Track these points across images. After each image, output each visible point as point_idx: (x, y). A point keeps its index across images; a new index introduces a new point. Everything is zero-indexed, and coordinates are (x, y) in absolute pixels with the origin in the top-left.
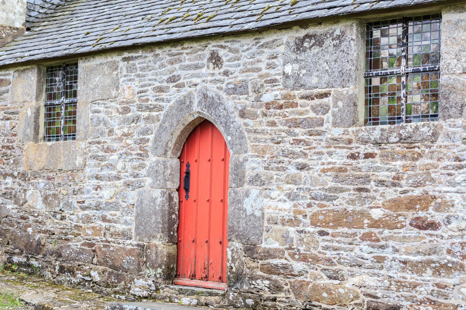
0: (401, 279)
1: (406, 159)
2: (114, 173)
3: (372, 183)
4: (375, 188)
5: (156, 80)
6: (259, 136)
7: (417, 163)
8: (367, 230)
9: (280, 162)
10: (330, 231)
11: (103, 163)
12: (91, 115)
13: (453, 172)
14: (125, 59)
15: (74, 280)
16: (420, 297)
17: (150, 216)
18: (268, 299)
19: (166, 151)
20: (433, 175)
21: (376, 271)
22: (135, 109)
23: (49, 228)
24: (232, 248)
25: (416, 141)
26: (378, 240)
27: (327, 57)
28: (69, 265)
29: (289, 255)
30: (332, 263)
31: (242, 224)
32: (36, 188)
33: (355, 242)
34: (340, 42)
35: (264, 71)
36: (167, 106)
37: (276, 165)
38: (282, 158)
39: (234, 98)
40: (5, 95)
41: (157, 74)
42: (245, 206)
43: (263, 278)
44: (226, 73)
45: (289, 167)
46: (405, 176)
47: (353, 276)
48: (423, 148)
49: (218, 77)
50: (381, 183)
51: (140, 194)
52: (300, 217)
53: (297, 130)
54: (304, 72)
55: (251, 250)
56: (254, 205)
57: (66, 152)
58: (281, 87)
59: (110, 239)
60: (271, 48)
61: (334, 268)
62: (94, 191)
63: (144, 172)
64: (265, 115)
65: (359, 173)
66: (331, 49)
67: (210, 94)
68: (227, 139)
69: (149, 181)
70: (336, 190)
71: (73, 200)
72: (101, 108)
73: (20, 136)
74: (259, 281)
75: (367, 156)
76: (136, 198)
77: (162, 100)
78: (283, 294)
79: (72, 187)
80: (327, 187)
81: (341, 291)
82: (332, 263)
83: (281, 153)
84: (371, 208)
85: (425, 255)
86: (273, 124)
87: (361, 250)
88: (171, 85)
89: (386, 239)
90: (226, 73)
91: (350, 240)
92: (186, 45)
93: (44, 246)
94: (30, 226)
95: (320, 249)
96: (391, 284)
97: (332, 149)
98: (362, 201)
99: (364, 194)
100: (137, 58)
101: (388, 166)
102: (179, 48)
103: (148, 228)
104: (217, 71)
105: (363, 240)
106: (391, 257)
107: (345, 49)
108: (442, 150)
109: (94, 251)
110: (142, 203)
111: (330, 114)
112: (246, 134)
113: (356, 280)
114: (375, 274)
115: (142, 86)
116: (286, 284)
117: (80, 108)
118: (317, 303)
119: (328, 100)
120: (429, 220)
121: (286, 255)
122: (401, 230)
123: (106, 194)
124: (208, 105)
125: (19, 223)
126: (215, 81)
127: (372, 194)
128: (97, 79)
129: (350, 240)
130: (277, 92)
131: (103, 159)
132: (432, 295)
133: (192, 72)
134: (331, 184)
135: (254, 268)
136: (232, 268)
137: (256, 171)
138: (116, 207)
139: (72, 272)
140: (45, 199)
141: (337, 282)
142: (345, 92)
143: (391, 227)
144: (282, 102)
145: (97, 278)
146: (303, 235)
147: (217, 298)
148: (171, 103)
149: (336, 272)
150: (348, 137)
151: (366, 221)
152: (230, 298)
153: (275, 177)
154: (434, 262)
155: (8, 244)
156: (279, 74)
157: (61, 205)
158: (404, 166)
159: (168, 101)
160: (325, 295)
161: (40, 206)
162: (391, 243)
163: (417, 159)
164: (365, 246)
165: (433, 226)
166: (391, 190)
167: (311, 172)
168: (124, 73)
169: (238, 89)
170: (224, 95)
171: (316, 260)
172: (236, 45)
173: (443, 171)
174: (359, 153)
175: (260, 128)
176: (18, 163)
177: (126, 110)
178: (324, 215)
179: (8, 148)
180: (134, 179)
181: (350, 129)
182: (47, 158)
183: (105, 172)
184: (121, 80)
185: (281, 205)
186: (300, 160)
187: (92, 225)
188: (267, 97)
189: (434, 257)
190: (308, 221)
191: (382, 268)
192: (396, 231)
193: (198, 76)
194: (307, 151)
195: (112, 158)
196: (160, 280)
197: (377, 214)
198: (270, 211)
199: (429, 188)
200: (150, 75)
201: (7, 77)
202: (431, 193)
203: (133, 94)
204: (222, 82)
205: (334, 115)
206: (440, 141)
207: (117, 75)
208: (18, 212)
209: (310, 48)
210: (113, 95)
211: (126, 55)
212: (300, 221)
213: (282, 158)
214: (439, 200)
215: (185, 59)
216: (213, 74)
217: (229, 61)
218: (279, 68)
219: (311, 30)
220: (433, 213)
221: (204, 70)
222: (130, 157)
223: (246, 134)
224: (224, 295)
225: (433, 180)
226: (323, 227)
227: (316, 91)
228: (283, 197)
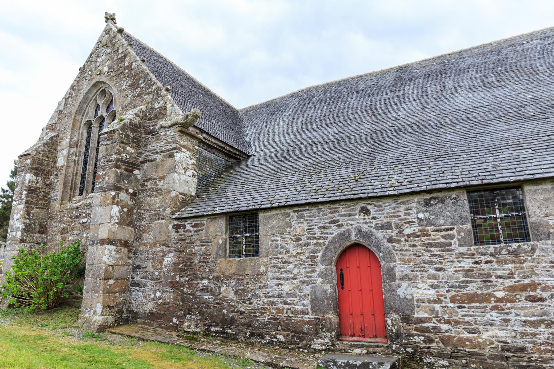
0: (524, 331)
1: (515, 263)
2: (292, 276)
3: (493, 277)
4: (496, 280)
5: (320, 222)
6: (404, 253)
7: (524, 265)
8: (494, 304)
9: (422, 267)
10: (466, 306)
11: (282, 270)
12: (270, 243)
13: (550, 269)
14: (295, 211)
15: (263, 341)
16: (539, 341)
17: (323, 301)
18: (424, 348)
19: (332, 262)
20: (537, 272)
21: (504, 327)
22: (305, 239)
23: (240, 309)
24: (391, 318)
25: (520, 253)
26: (503, 310)
27: (449, 209)
28: (259, 332)
29: (437, 320)
30: (470, 324)
31: (398, 303)
32: (229, 286)
33: (486, 311)
34: (457, 201)
35: (403, 217)
36: (330, 237)
37: (419, 269)
38: (423, 265)
39: (382, 232)
40: (201, 232)
41: (321, 219)
42: (398, 293)
43: (419, 335)
44: (374, 218)
45: (430, 270)
46: (517, 273)
47: (487, 331)
48: (526, 257)
49: (368, 220)
50: (500, 277)
51: (312, 288)
52: (442, 298)
53: (432, 249)
54: (433, 217)
55: (407, 319)
56: (405, 292)
57: (252, 264)
58: (417, 225)
59: (291, 315)
60: (406, 204)
61: (473, 327)
62: (276, 287)
63: (315, 274)
64: (407, 241)
65: (483, 272)
66: (451, 205)
67: (364, 230)
68: (379, 255)
69: (320, 280)
70: (467, 282)
71: (260, 292)
72: (279, 238)
73: (213, 255)
74: (415, 337)
75: (487, 262)
76: (310, 290)
77: (327, 233)
78: (435, 344)
79: (258, 284)
80: (460, 280)
81: (480, 340)
82: (470, 324)
83: (422, 262)
84: (494, 291)
85: (538, 316)
86: (414, 246)
87: (492, 316)
88: (332, 225)
89: (509, 308)
90: (374, 218)
91: (483, 310)
92: (342, 203)
93: (236, 320)
94: (225, 308)
95: (460, 316)
96: (516, 335)
97: (461, 259)
98: (487, 288)
99: (489, 284)
100: (304, 210)
101: (503, 267)
102: (337, 205)
103: (322, 308)
104: (366, 217)
105: (492, 310)
106: (514, 319)
107: (461, 205)
108: (540, 257)
109: (279, 323)
110: (315, 292)
111: (455, 239)
112: (394, 252)
113: (490, 333)
114: (504, 329)
115: (310, 226)
116: (437, 338)
117: (262, 239)
118: (462, 348)
119: (454, 232)
120: (539, 296)
121: (434, 320)
122: (519, 303)
123: (286, 288)
124: (362, 235)
125: (215, 307)
126: (366, 223)
127: (494, 283)
128: (274, 222)
129: (483, 310)
130: (415, 228)
131: (282, 268)
132: (548, 339)
133: (348, 218)
134: (462, 279)
135: (410, 329)
136: (392, 330)
137: (404, 273)
138: (295, 295)
139: (262, 336)
140: (236, 293)
141: (475, 335)
142: (465, 228)
143: (511, 301)
144: (419, 234)
145: (283, 339)
146: (446, 309)
147: (382, 348)
148: (334, 235)
149: (473, 329)
150: (471, 252)
151: (492, 299)
152: (394, 348)
153: (420, 276)
154: (546, 321)
155: (206, 319)
156: (415, 219)
157: (250, 295)
158: (515, 267)
159: (331, 234)
160: (467, 343)
161: (232, 296)
162: (513, 311)
163: (523, 263)
164: (494, 313)
165: (542, 300)
166: (508, 280)
167: (447, 272)
168: (296, 218)
169: (386, 227)
170: (374, 231)
171: (457, 323)
172: (380, 203)
173: (542, 269)
174: (481, 261)
175: (404, 248)
176: (213, 271)
177: (298, 240)
178: (461, 296)
179: (204, 262)
180: (307, 279)
181: (472, 248)
182: (236, 268)
183: (284, 275)
184: (293, 223)
185: (426, 292)
186: (437, 266)
187: (276, 307)
188: (408, 231)
189: (545, 317)
190: (448, 300)
191: (507, 326)
192: (515, 303)
193: (353, 220)
194: (442, 261)
195: (289, 267)
196: (334, 339)
197: (500, 294)
198: (418, 295)
199: (534, 278)
200: (315, 220)
201: (202, 222)
202: (537, 282)
203: (303, 230)
204: (372, 223)
205: (458, 240)
206: (537, 252)
207: (290, 220)
208: (214, 300)
209: (436, 204)
210: (288, 231)
211: (296, 209)
212: (442, 301)
213: (423, 265)
214: (543, 285)
215: (342, 211)
216: (364, 219)
217: (375, 211)
218: (414, 215)
219: (435, 195)
220: (541, 292)
221: (357, 217)
222: (303, 266)
223: (394, 252)
224: (388, 347)
225: (537, 274)
226: (460, 303)
227: (443, 227)
228: (427, 287)
